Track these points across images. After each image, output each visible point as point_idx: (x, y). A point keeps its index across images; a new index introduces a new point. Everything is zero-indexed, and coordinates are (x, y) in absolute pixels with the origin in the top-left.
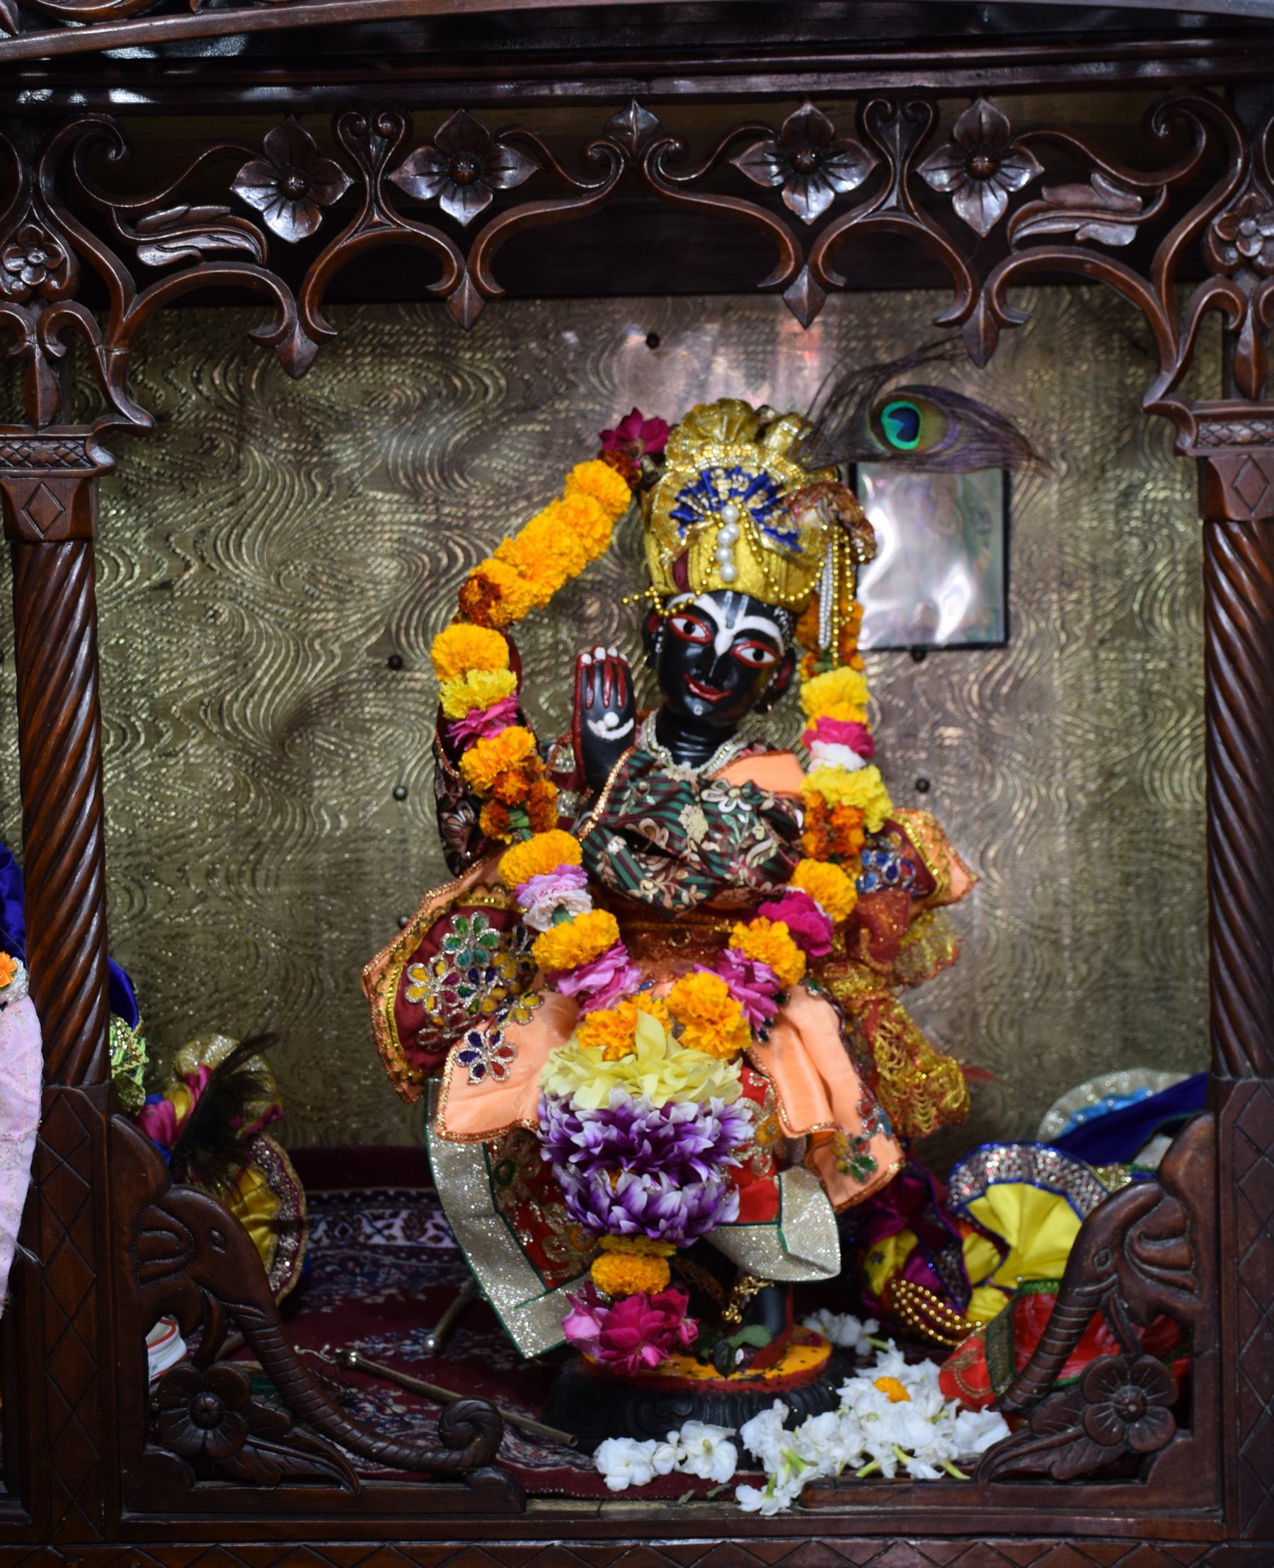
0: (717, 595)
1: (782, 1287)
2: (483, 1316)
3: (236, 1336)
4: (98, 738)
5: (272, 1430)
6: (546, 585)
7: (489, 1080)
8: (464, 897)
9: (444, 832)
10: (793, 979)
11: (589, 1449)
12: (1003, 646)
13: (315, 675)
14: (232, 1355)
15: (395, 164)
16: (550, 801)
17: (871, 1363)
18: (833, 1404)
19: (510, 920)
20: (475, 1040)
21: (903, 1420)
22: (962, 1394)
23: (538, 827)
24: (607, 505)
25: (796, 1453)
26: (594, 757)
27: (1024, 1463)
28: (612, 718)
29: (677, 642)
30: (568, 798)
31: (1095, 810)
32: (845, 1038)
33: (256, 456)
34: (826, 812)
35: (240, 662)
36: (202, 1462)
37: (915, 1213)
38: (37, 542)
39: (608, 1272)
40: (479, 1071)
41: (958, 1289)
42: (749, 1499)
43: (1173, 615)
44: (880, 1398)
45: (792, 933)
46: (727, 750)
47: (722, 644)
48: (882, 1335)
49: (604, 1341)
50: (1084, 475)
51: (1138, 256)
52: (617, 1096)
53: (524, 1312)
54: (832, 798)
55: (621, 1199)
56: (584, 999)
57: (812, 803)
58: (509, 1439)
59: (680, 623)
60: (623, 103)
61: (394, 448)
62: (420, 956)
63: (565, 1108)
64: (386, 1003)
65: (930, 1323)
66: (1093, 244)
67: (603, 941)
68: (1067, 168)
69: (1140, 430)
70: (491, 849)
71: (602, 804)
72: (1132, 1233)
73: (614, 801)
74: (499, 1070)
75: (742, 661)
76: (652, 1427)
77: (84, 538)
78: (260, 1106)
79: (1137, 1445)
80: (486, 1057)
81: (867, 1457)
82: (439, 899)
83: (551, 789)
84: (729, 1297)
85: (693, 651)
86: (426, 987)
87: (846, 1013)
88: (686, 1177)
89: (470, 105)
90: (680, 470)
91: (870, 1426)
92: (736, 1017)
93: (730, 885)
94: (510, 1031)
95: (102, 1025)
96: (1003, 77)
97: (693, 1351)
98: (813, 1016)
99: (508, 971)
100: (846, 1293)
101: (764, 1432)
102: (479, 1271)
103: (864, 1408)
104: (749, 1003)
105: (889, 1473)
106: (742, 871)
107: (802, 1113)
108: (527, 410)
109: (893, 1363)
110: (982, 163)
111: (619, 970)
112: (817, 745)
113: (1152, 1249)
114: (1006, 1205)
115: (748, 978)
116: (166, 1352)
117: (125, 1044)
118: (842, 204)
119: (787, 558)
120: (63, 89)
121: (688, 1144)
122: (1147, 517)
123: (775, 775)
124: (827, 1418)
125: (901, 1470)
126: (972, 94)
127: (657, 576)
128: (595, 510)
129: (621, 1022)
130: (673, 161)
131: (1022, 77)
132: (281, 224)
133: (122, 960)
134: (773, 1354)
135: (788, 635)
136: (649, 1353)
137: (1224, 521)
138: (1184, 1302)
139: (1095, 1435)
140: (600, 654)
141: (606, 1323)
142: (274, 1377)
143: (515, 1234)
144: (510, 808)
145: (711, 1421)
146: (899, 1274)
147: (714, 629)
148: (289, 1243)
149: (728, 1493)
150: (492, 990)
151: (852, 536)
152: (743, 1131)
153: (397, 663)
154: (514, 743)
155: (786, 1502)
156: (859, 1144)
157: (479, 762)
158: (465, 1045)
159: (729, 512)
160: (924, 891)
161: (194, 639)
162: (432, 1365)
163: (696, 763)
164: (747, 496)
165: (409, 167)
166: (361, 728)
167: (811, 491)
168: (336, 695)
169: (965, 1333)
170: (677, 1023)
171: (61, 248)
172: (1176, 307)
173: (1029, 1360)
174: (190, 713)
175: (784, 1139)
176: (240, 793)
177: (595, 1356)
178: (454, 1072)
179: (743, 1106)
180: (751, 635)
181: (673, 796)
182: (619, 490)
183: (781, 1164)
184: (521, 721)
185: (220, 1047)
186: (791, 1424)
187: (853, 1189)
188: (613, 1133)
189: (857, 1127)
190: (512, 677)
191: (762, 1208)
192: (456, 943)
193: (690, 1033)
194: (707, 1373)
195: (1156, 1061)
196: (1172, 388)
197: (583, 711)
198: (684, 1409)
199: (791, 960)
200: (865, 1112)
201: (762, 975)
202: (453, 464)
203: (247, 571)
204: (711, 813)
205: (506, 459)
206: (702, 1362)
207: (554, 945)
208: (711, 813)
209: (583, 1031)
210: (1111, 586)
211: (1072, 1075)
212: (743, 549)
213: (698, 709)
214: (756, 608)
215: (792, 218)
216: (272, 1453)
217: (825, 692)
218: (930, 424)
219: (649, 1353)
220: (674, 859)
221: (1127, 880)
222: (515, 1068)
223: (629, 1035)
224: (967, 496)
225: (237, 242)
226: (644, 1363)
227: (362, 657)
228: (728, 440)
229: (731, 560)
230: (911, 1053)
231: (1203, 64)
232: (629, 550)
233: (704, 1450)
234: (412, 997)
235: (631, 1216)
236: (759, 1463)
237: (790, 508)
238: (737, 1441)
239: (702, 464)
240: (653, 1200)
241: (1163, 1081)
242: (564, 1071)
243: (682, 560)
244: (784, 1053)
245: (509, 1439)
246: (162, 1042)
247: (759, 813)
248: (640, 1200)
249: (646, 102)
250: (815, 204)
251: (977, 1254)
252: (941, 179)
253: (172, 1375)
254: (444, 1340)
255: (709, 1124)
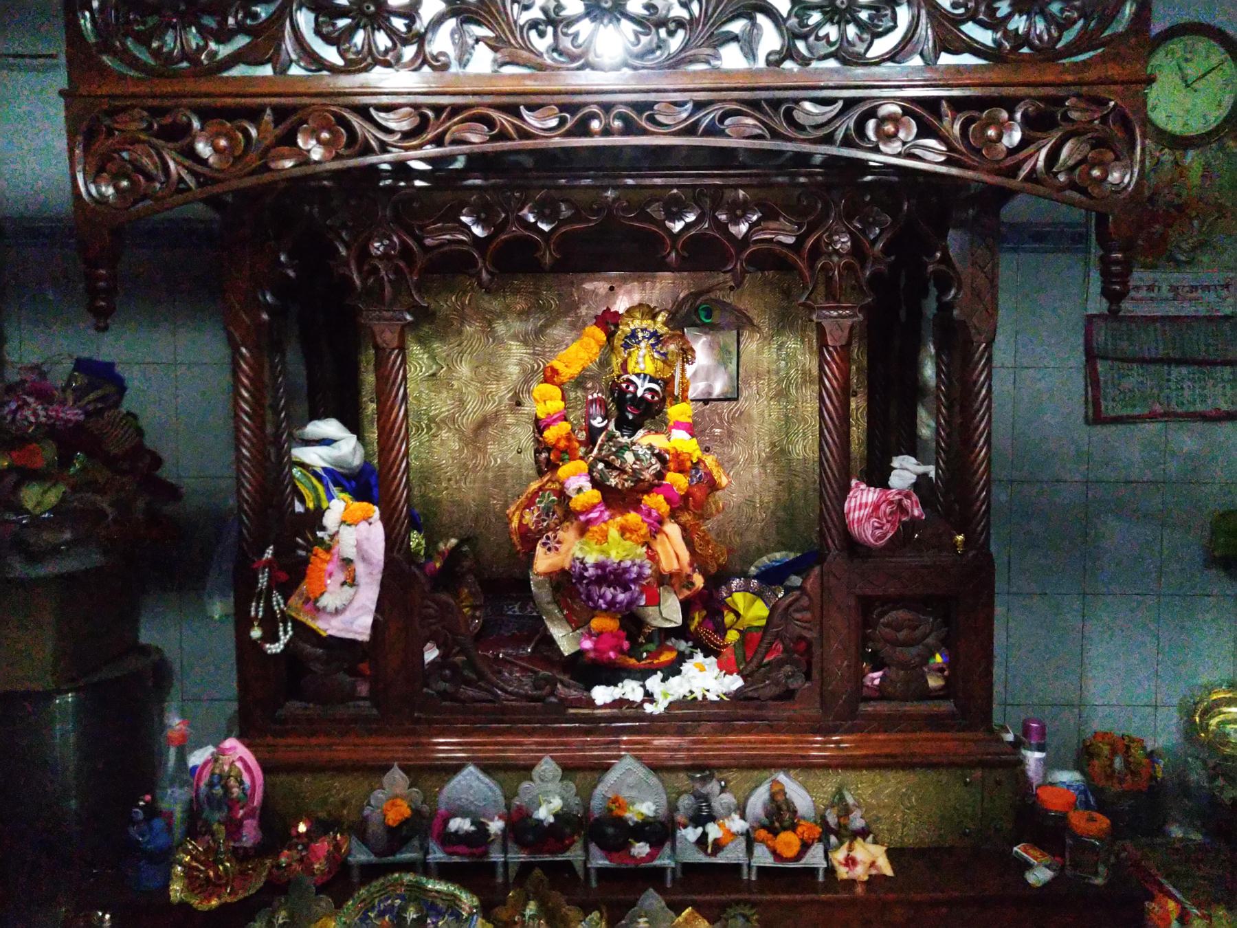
0: (638, 375)
1: (661, 629)
2: (551, 641)
3: (457, 648)
4: (407, 429)
5: (469, 683)
6: (575, 370)
7: (552, 553)
8: (544, 485)
9: (537, 461)
10: (665, 515)
11: (589, 689)
12: (736, 399)
13: (490, 408)
14: (456, 655)
15: (521, 209)
16: (576, 449)
17: (691, 656)
18: (679, 672)
19: (563, 496)
20: (548, 538)
21: (705, 679)
22: (726, 669)
23: (572, 459)
24: (597, 342)
25: (665, 692)
26: (593, 433)
27: (750, 694)
28: (599, 419)
29: (623, 392)
30: (583, 449)
31: (768, 458)
32: (684, 538)
33: (468, 329)
34: (677, 455)
35: (462, 403)
36: (443, 695)
37: (707, 605)
38: (384, 349)
39: (596, 623)
40: (549, 549)
41: (722, 630)
42: (649, 708)
43: (797, 389)
44: (696, 670)
45: (666, 499)
46: (641, 432)
47: (640, 393)
48: (694, 647)
49: (595, 650)
50: (765, 338)
51: (796, 247)
52: (601, 558)
53: (565, 639)
54: (679, 450)
55: (602, 596)
56: (589, 522)
57: (672, 451)
58: (559, 686)
59: (624, 386)
60: (606, 188)
61: (517, 326)
62: (528, 506)
63: (582, 563)
64: (515, 524)
65: (712, 642)
66: (780, 243)
67: (596, 501)
68: (769, 214)
69: (785, 321)
70: (553, 467)
71: (596, 451)
72: (791, 609)
73: (600, 450)
74: (557, 549)
75: (647, 400)
76: (612, 681)
77: (402, 348)
78: (466, 564)
79: (791, 687)
80: (552, 544)
81: (692, 692)
82: (534, 486)
83: (577, 445)
84: (640, 633)
85: (629, 396)
86: (530, 518)
87: (684, 528)
88: (626, 589)
89: (549, 188)
90: (625, 329)
91: (693, 681)
92: (644, 529)
93: (643, 481)
94: (561, 534)
95: (408, 532)
96: (745, 181)
97: (630, 653)
98: (672, 529)
99: (559, 513)
100: (681, 632)
101: (654, 683)
102: (549, 624)
103: (691, 674)
104: (650, 525)
105: (700, 698)
106: (647, 475)
107: (668, 564)
108: (566, 314)
109: (699, 657)
110: (739, 212)
111: (602, 512)
112: (674, 431)
113: (798, 616)
114: (739, 600)
115: (649, 514)
116: (431, 654)
117: (416, 539)
118: (688, 226)
119: (664, 362)
120: (397, 180)
121: (627, 576)
122: (787, 354)
123: (659, 441)
124: (677, 678)
125: (704, 696)
126: (736, 187)
127: (616, 369)
128: (593, 343)
129: (602, 530)
130: (624, 210)
131: (755, 181)
132: (477, 231)
133: (417, 510)
134: (657, 654)
135: (664, 390)
136: (612, 654)
137: (827, 346)
138: (808, 635)
139: (777, 683)
140: (595, 396)
141: (596, 643)
142: (471, 664)
143: (561, 611)
144: (562, 452)
145: (634, 679)
146: (700, 624)
147: (637, 388)
148: (478, 614)
149: (641, 705)
150: (553, 520)
151: (686, 354)
152: (648, 572)
153: (519, 404)
154: (564, 427)
155: (662, 710)
156: (689, 576)
157: (550, 434)
158: (544, 540)
159: (643, 344)
160: (713, 486)
161: (444, 395)
162: (529, 658)
163: (630, 437)
164: (649, 339)
165: (525, 211)
166: (505, 427)
167: (672, 337)
168: (497, 415)
169: (726, 646)
170: (623, 530)
171: (395, 239)
172: (811, 267)
173: (748, 656)
174: (443, 421)
175: (661, 574)
176: (461, 450)
177: (592, 655)
178: (540, 550)
179: (648, 563)
180: (650, 390)
181: (622, 448)
182: (602, 337)
183: (660, 584)
184: (566, 420)
185: (453, 541)
186: (664, 680)
187: (687, 593)
188: (599, 572)
189: (688, 570)
190: (562, 404)
191: (655, 601)
192: (540, 502)
193: (628, 535)
194: (633, 661)
195: (791, 549)
196: (808, 298)
197: (589, 417)
198: (624, 675)
199: (665, 508)
200: (691, 565)
201: (654, 514)
202: (540, 332)
203: (464, 370)
204: (636, 455)
205: (557, 332)
206: (631, 657)
207: (578, 502)
208: (636, 455)
209: (589, 534)
210: (775, 378)
211: (760, 553)
212: (648, 358)
213: (631, 417)
214: (652, 380)
215: (669, 231)
216: (471, 692)
217: (677, 412)
218: (716, 313)
219: (612, 654)
220: (622, 471)
221: (780, 483)
222: (563, 548)
223: (605, 536)
224: (725, 345)
225: (461, 237)
226: (610, 658)
227: (506, 401)
228: (642, 319)
229: (643, 362)
230: (708, 543)
231: (820, 178)
232: (604, 363)
233: (631, 690)
234: (524, 522)
235: (606, 603)
236: (652, 695)
237: (664, 343)
238: (644, 686)
239: (632, 327)
240: (614, 597)
241: (792, 556)
242: (581, 549)
243: (625, 363)
244: (663, 543)
245: (559, 686)
246: (431, 542)
247: (653, 454)
248: (609, 596)
249: (615, 188)
250: (677, 226)
251: (729, 618)
252: (723, 217)
253: (433, 662)
254: (533, 650)
255: (635, 569)
